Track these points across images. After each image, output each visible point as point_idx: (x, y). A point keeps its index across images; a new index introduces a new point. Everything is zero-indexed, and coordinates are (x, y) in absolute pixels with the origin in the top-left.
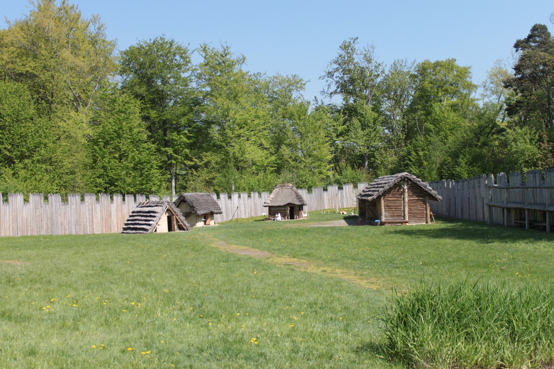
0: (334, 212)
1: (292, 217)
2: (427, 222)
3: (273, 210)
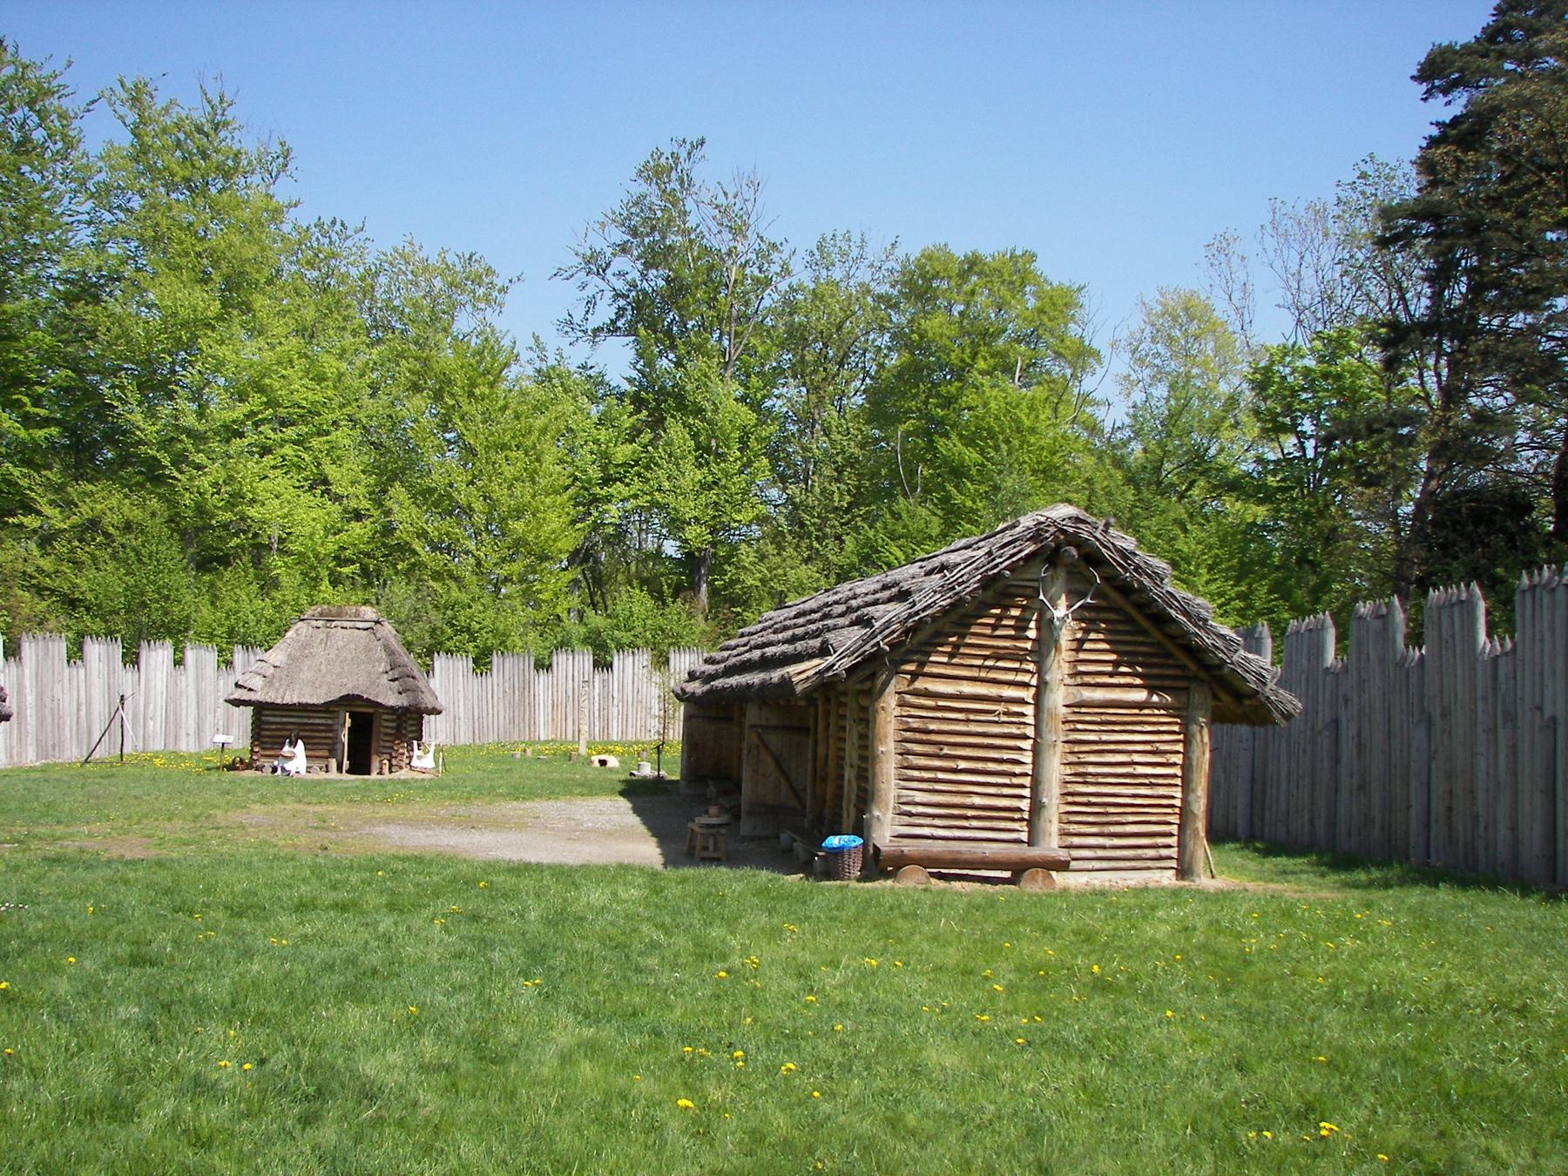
0: (569, 756)
1: (360, 766)
2: (1183, 871)
3: (273, 725)
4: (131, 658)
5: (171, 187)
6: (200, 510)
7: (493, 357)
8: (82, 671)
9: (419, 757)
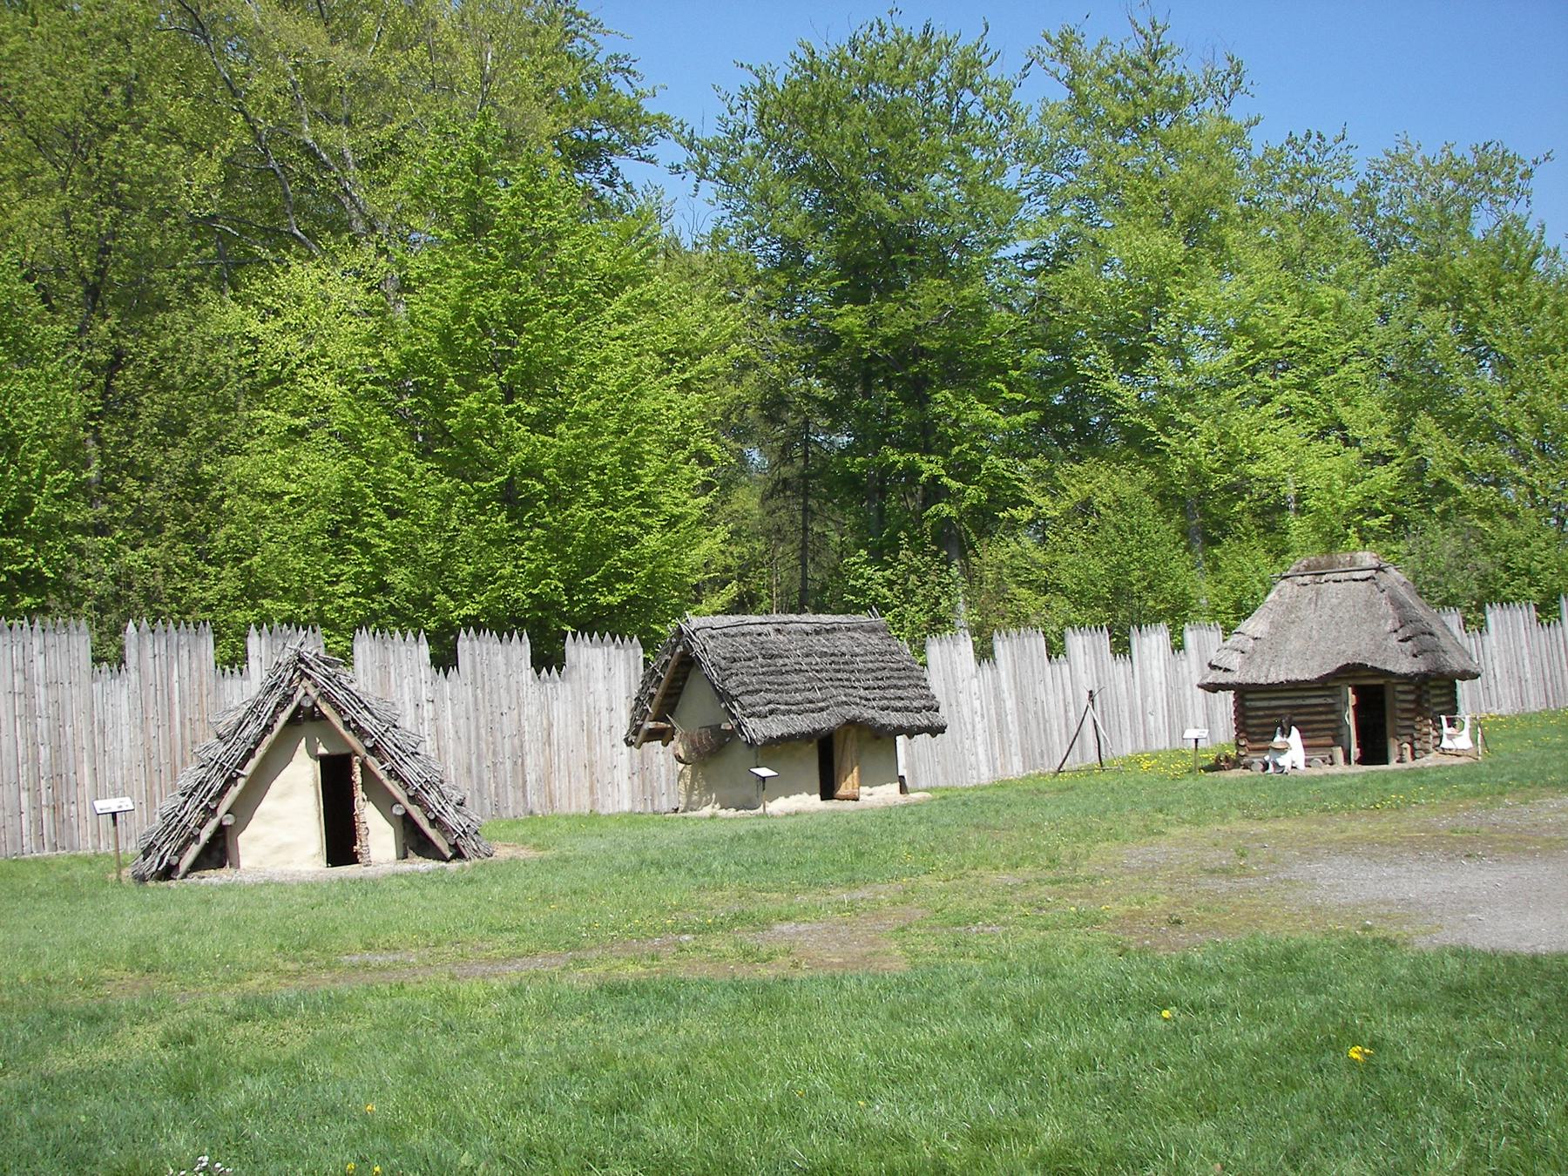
1: (1373, 752)
3: (1261, 710)
4: (1121, 647)
5: (1117, 133)
6: (1195, 474)
7: (1518, 249)
8: (1066, 668)
9: (1451, 737)
